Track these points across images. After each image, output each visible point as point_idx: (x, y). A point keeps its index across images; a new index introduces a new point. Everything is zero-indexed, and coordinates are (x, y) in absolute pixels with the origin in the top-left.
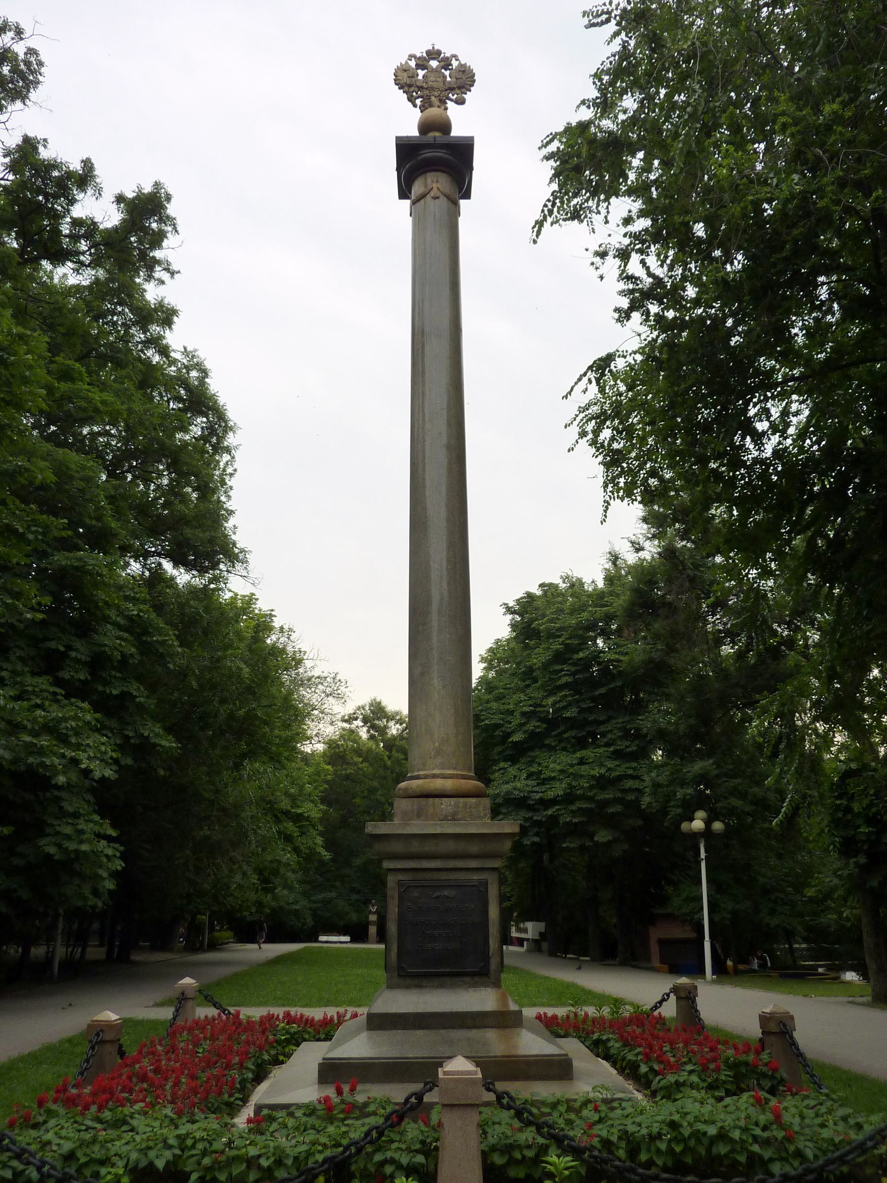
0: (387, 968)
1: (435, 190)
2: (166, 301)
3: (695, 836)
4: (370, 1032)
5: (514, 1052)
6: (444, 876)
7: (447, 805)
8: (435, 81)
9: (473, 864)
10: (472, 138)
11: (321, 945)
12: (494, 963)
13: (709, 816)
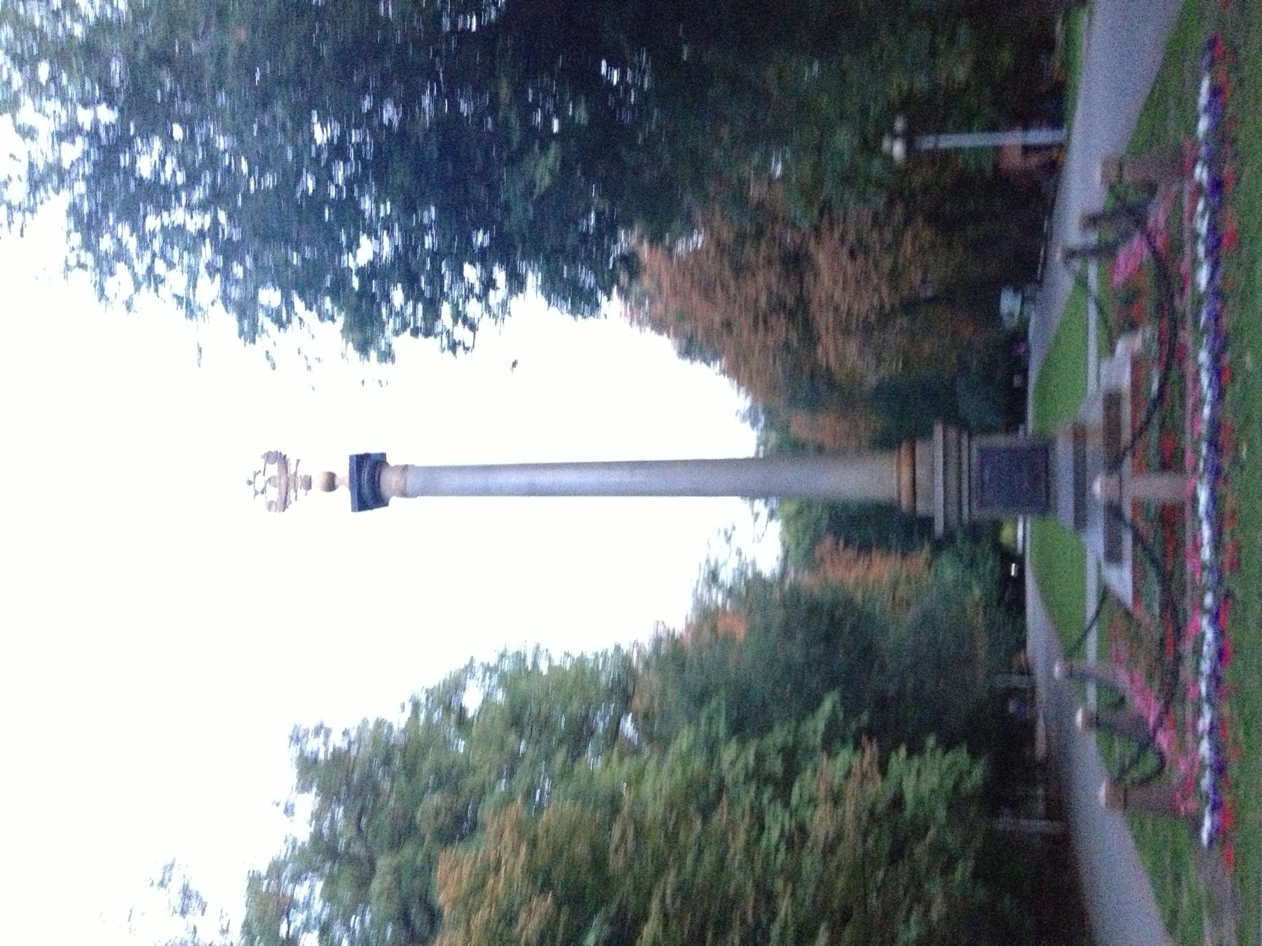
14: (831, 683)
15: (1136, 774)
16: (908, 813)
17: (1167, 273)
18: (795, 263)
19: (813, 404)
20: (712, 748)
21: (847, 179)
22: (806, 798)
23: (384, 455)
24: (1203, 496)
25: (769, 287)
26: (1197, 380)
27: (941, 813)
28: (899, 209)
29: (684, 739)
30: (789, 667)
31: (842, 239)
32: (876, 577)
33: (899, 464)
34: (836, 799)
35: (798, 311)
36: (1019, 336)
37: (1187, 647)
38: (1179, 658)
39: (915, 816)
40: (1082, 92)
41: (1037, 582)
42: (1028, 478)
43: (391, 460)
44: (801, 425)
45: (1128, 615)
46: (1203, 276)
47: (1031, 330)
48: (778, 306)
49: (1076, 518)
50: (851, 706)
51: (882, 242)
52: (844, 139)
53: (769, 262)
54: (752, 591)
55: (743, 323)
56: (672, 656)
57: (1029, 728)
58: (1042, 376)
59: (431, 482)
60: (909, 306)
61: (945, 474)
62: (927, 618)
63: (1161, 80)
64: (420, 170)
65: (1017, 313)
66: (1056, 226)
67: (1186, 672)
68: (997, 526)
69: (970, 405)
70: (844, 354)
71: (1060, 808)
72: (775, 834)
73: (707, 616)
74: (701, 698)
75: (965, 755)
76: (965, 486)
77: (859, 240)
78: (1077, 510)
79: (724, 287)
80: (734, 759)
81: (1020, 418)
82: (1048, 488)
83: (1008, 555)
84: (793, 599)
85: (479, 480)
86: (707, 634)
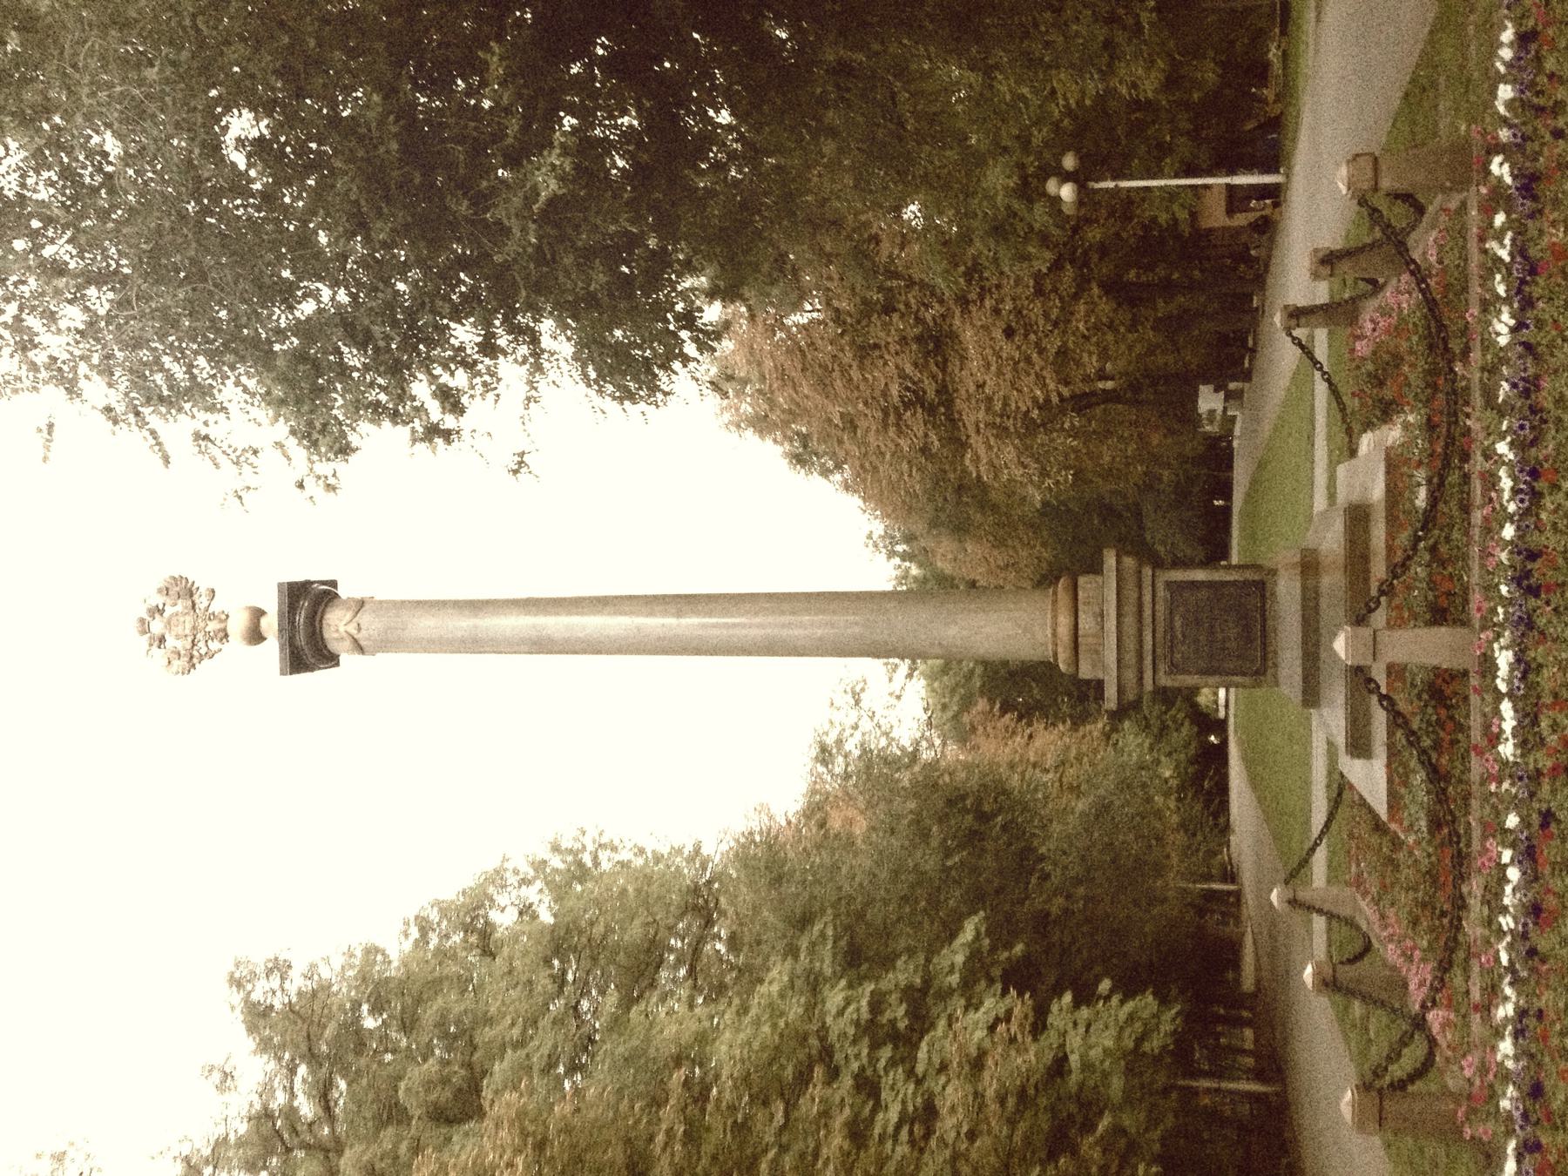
0: (1257, 685)
2: (281, 958)
4: (1323, 702)
5: (1341, 561)
7: (1087, 623)
8: (183, 620)
9: (1147, 598)
11: (1232, 712)
12: (1250, 575)
13: (1055, 175)
14: (976, 900)
15: (1397, 1071)
16: (1074, 1078)
17: (1442, 331)
18: (937, 345)
19: (961, 529)
20: (815, 984)
21: (999, 230)
22: (936, 1061)
23: (334, 584)
24: (1504, 659)
25: (903, 376)
26: (1491, 481)
27: (1117, 1084)
28: (1069, 272)
29: (778, 974)
30: (921, 877)
31: (996, 311)
32: (1037, 752)
33: (1055, 602)
34: (977, 1064)
35: (939, 407)
36: (1218, 454)
37: (1474, 888)
38: (1460, 904)
39: (1081, 1086)
40: (1307, 119)
42: (1236, 629)
43: (343, 592)
44: (946, 554)
45: (1378, 827)
46: (1503, 326)
47: (1237, 431)
48: (914, 399)
49: (1305, 692)
51: (1046, 315)
52: (998, 178)
53: (903, 340)
54: (877, 772)
55: (869, 422)
56: (766, 860)
59: (402, 627)
60: (1082, 403)
61: (1119, 616)
62: (1103, 809)
63: (1428, 60)
64: (374, 176)
65: (1220, 411)
66: (1267, 304)
67: (1473, 929)
68: (1195, 691)
69: (1160, 532)
70: (995, 460)
71: (1274, 1064)
73: (816, 810)
74: (804, 921)
75: (1151, 998)
76: (1148, 638)
77: (1018, 312)
78: (1305, 679)
79: (844, 371)
80: (842, 1006)
81: (1225, 554)
82: (1264, 645)
83: (1209, 723)
84: (930, 782)
85: (463, 624)
86: (810, 832)
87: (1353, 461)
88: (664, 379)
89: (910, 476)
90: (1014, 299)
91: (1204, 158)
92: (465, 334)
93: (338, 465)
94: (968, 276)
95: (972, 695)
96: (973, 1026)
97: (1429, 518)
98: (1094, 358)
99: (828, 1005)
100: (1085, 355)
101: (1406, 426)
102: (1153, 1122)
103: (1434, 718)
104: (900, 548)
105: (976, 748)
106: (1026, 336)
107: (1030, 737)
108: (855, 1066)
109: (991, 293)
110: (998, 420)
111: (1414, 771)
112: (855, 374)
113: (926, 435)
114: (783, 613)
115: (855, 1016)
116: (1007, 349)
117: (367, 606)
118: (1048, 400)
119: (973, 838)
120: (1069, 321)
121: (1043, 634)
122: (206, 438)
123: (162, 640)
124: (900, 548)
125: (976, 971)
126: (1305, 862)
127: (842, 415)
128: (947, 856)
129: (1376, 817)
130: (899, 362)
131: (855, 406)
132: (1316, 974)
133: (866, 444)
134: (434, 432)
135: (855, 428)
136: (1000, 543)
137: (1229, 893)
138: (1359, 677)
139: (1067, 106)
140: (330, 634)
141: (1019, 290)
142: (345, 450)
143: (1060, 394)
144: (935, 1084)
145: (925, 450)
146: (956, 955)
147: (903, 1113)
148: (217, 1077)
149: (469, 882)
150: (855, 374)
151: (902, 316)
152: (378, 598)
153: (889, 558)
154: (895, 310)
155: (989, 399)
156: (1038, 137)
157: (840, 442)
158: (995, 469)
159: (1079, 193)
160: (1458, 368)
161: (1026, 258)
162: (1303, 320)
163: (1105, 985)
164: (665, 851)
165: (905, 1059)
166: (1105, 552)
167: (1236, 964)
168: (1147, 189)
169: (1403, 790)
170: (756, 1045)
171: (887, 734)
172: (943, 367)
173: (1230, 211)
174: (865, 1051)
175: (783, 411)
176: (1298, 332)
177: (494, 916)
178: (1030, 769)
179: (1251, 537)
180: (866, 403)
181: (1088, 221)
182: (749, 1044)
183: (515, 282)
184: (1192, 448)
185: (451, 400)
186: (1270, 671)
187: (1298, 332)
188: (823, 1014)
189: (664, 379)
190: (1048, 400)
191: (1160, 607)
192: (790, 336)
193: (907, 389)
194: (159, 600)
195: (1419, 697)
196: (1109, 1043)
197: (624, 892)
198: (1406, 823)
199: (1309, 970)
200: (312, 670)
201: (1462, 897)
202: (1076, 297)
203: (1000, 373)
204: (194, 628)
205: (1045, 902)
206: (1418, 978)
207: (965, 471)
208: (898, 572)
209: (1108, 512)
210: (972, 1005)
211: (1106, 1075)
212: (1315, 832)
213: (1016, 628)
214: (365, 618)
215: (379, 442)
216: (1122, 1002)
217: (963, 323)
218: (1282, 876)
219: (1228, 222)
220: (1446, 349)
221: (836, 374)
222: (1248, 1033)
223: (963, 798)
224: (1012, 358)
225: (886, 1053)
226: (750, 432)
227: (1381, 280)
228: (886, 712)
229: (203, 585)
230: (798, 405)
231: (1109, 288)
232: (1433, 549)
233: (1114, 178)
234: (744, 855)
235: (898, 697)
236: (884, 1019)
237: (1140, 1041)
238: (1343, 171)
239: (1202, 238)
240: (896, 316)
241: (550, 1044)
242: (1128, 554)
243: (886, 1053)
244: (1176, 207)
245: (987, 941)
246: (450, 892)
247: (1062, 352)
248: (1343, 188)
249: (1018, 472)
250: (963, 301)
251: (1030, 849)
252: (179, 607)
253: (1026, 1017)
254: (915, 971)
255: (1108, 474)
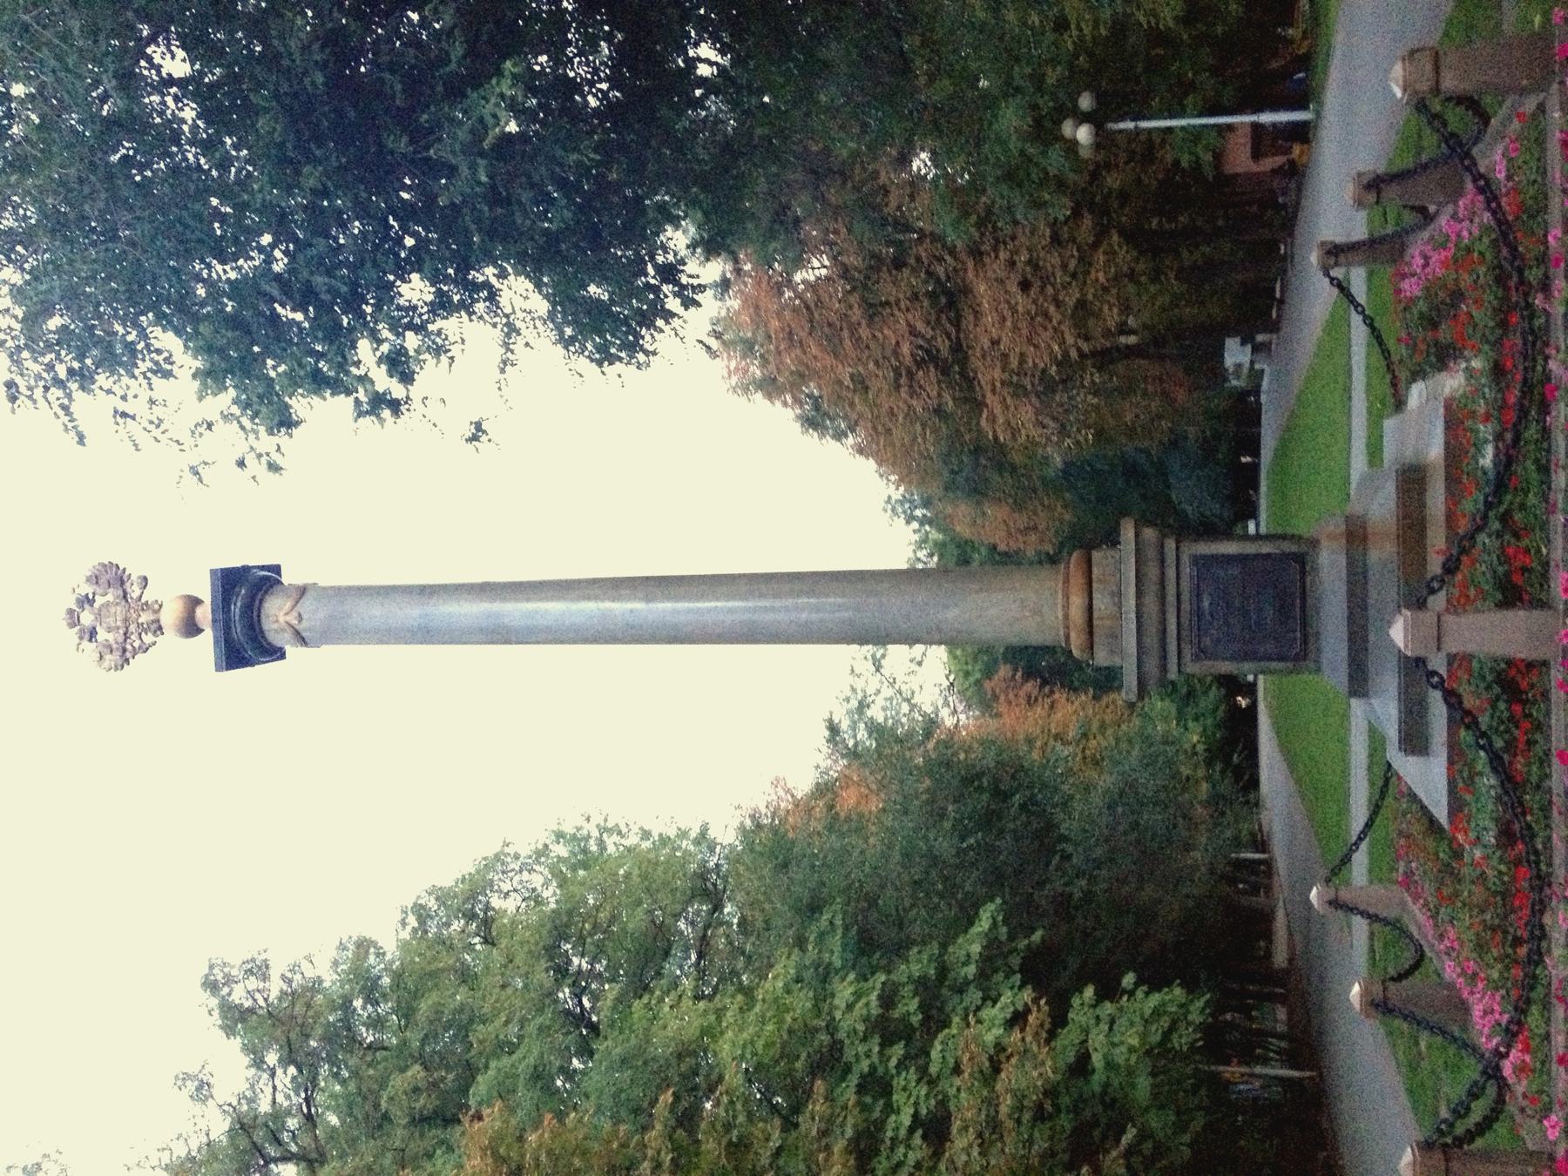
1: (288, 618)
3: (1103, 139)
6: (1186, 606)
7: (1101, 603)
8: (113, 613)
9: (1171, 573)
10: (213, 572)
16: (1098, 1078)
18: (950, 301)
19: (978, 491)
21: (1010, 177)
23: (277, 569)
27: (1143, 1083)
28: (1087, 221)
33: (1067, 581)
35: (953, 365)
39: (1107, 1085)
40: (1339, 40)
41: (1273, 724)
43: (286, 579)
50: (1019, 917)
51: (1064, 266)
52: (1011, 119)
53: (915, 297)
55: (880, 382)
56: (771, 844)
57: (1264, 920)
58: (1282, 452)
59: (351, 614)
60: (1104, 358)
61: (1139, 594)
62: (1127, 794)
64: (298, 110)
65: (1247, 365)
70: (1014, 420)
71: (1308, 1045)
72: (906, 1120)
74: (814, 908)
77: (1033, 263)
79: (854, 329)
82: (1304, 625)
85: (411, 612)
87: (1400, 417)
88: (648, 338)
89: (924, 438)
90: (1029, 250)
91: (1228, 95)
92: (415, 290)
93: (282, 438)
94: (980, 225)
95: (996, 661)
96: (990, 1027)
97: (1503, 480)
98: (1115, 310)
99: (837, 1002)
100: (1106, 307)
101: (1470, 373)
102: (1181, 1127)
103: (1506, 714)
104: (918, 513)
105: (998, 715)
106: (1043, 288)
107: (1052, 707)
108: (865, 1065)
109: (1005, 243)
110: (1015, 378)
111: (1481, 774)
112: (864, 332)
113: (939, 395)
114: (761, 596)
115: (865, 1012)
116: (1022, 302)
117: (308, 595)
118: (1066, 354)
119: (989, 820)
120: (1089, 273)
121: (1054, 616)
122: (124, 415)
123: (93, 634)
124: (918, 513)
125: (991, 961)
126: (1346, 860)
127: (852, 376)
128: (963, 839)
129: (1432, 821)
130: (910, 317)
131: (865, 365)
132: (1365, 992)
133: (879, 406)
134: (381, 403)
135: (867, 388)
136: (1018, 506)
137: (1260, 862)
138: (1414, 668)
139: (1081, 37)
140: (269, 626)
141: (1035, 240)
142: (285, 422)
143: (1079, 349)
144: (950, 1086)
145: (938, 411)
146: (972, 945)
147: (915, 1116)
148: (191, 1086)
149: (469, 868)
150: (864, 332)
151: (913, 270)
152: (322, 584)
153: (908, 522)
154: (905, 264)
155: (1005, 356)
156: (1052, 76)
157: (852, 405)
158: (1015, 433)
159: (1097, 134)
160: (1538, 301)
161: (1038, 205)
162: (1342, 258)
163: (1128, 980)
164: (672, 833)
165: (918, 1056)
166: (1123, 522)
167: (1268, 935)
168: (1169, 130)
169: (1468, 797)
170: (760, 1044)
171: (908, 700)
172: (957, 325)
173: (1256, 155)
174: (876, 1049)
175: (792, 373)
176: (1337, 273)
177: (496, 902)
178: (1052, 742)
179: (1280, 491)
180: (877, 363)
181: (1108, 166)
182: (752, 1043)
183: (466, 230)
184: (1219, 404)
185: (399, 365)
186: (1312, 656)
187: (1337, 273)
188: (833, 1008)
189: (648, 338)
190: (1066, 354)
191: (1186, 584)
192: (798, 296)
193: (921, 347)
194: (87, 589)
195: (1488, 688)
196: (1135, 1042)
197: (628, 876)
198: (1472, 835)
199: (1356, 989)
200: (252, 665)
201: (1542, 927)
202: (1095, 246)
203: (1016, 328)
204: (126, 620)
205: (1066, 885)
206: (1485, 1016)
207: (980, 431)
208: (916, 537)
209: (1132, 471)
210: (991, 998)
211: (1131, 1072)
212: (1364, 846)
213: (1030, 608)
214: (307, 605)
215: (323, 414)
216: (1147, 994)
217: (977, 276)
218: (1324, 873)
219: (1254, 168)
220: (1522, 281)
221: (846, 333)
222: (1282, 1014)
223: (979, 776)
224: (1028, 313)
225: (898, 1050)
226: (759, 395)
227: (1432, 208)
228: (907, 679)
229: (134, 571)
230: (807, 367)
231: (1129, 237)
232: (1505, 518)
233: (1133, 120)
234: (753, 832)
235: (920, 664)
236: (896, 1014)
237: (1167, 1035)
238: (1398, 70)
239: (1225, 181)
240: (906, 272)
241: (536, 1053)
242: (1151, 523)
243: (898, 1050)
244: (1199, 150)
245: (1004, 930)
246: (447, 878)
247: (1082, 304)
248: (1399, 93)
249: (1035, 432)
250: (976, 253)
251: (1050, 826)
252: (110, 598)
253: (1042, 1025)
254: (929, 961)
255: (1131, 432)
